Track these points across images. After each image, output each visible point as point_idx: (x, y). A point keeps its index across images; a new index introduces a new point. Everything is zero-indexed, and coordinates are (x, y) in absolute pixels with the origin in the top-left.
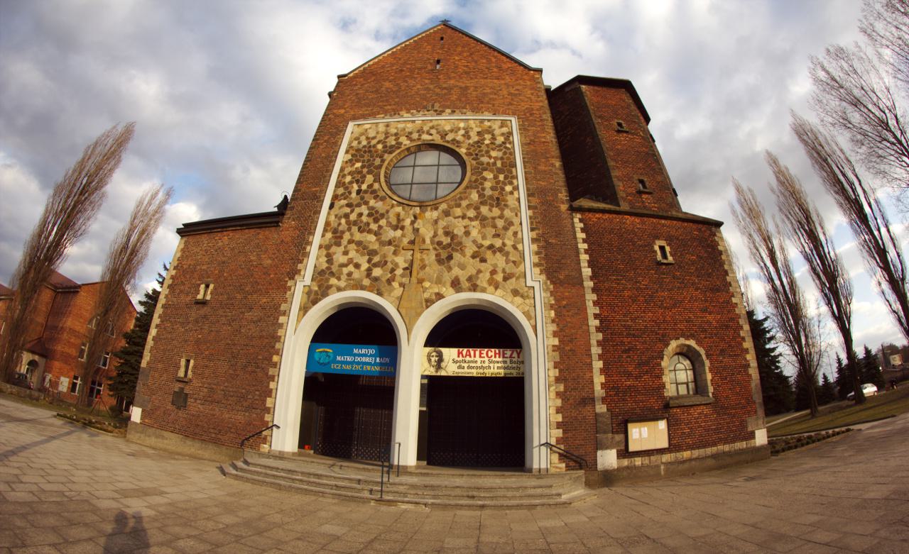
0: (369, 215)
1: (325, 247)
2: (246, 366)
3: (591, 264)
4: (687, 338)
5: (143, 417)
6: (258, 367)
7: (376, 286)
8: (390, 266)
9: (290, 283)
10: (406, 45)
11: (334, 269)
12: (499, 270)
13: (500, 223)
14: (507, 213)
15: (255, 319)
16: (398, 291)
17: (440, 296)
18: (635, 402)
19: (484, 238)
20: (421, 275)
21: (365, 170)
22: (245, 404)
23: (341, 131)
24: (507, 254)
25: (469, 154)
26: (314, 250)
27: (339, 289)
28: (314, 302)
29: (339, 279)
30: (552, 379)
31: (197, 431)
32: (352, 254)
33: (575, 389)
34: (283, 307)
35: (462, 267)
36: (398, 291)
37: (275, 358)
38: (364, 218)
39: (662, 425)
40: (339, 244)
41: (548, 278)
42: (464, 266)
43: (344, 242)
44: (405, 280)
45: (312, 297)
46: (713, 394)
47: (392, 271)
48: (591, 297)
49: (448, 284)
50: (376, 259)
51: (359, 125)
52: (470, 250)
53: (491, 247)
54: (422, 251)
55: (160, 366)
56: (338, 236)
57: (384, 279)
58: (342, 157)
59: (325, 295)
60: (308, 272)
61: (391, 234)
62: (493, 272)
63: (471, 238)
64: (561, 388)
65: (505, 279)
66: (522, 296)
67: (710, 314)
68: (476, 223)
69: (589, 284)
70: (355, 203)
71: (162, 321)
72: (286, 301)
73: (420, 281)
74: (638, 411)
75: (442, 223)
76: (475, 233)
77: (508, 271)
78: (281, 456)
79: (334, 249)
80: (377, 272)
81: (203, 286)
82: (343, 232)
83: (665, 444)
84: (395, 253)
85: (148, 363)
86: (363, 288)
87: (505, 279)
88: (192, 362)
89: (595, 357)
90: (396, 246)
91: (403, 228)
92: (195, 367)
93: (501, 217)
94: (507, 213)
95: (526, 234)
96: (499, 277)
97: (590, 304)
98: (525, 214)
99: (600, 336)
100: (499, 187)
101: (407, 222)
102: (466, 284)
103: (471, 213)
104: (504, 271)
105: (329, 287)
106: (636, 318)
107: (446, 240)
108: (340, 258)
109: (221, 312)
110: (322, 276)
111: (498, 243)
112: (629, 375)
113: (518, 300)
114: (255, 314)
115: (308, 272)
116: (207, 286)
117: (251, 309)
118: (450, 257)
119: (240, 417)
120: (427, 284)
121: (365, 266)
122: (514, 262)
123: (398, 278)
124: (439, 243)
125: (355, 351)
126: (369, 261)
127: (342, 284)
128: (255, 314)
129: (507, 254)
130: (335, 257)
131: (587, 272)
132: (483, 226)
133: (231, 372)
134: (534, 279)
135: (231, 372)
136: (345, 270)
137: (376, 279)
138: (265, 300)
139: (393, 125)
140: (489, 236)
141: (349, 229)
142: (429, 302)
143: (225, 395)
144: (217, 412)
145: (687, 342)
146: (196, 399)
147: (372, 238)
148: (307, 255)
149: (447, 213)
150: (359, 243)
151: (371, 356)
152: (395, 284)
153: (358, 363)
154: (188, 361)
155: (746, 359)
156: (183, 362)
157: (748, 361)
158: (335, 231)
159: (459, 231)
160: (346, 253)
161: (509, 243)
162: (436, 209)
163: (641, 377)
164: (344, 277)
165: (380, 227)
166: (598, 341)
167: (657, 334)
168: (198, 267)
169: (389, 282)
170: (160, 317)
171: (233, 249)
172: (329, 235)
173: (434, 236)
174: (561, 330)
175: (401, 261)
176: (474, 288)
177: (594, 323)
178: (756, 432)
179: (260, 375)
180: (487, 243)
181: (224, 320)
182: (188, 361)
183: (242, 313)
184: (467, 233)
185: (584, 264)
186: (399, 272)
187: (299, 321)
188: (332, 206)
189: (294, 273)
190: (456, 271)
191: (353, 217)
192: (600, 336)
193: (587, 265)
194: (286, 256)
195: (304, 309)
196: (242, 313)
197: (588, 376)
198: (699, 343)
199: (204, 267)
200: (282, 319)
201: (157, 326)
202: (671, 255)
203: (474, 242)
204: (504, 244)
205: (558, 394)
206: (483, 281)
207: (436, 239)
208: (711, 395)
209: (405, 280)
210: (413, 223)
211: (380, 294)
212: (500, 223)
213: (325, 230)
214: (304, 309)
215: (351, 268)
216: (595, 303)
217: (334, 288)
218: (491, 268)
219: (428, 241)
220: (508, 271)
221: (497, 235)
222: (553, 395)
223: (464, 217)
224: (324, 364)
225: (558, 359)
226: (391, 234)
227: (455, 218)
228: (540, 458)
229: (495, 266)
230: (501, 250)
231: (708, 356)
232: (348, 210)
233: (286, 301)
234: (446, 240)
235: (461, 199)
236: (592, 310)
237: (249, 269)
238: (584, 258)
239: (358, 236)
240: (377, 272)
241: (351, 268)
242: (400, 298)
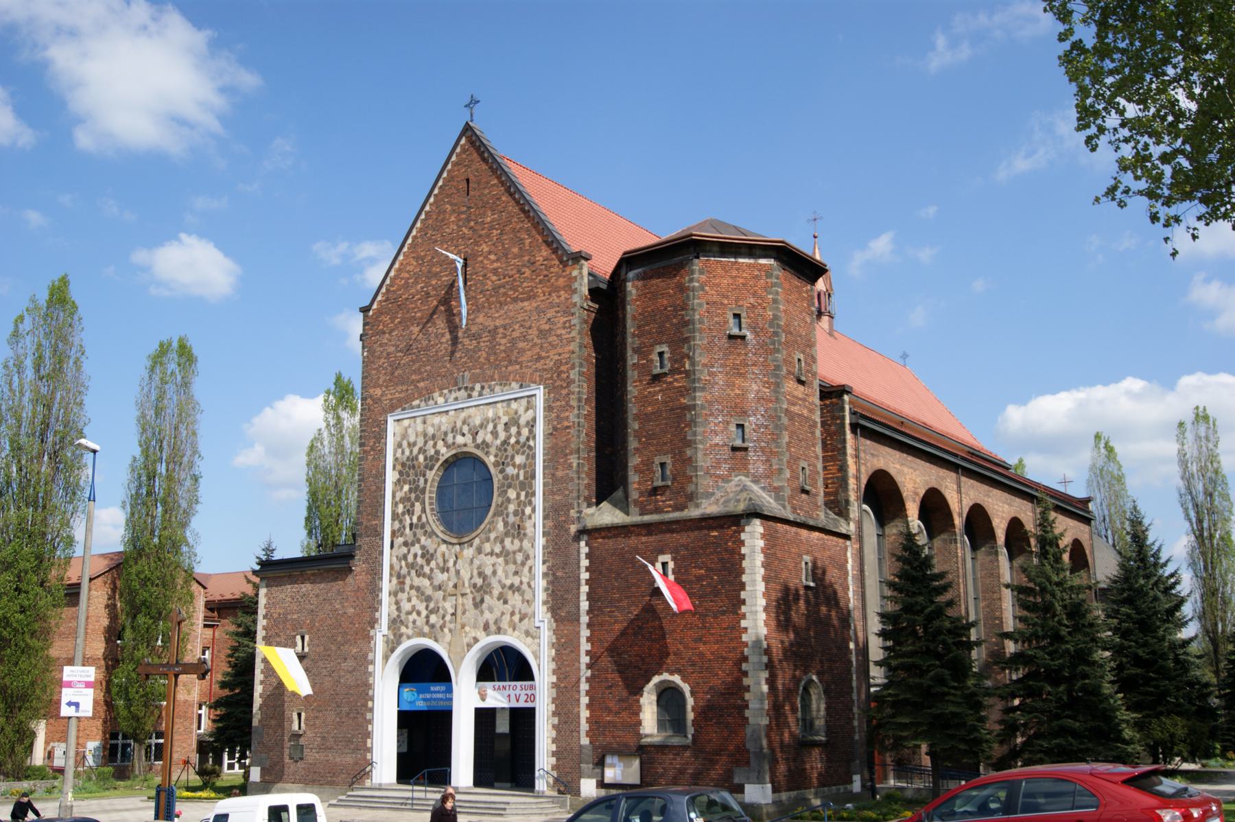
0: (423, 556)
1: (393, 594)
2: (348, 714)
3: (590, 597)
4: (672, 673)
5: (262, 775)
6: (358, 713)
7: (434, 634)
8: (441, 611)
9: (372, 633)
10: (427, 213)
11: (403, 617)
12: (517, 611)
13: (519, 557)
14: (526, 544)
15: (350, 669)
16: (448, 637)
17: (476, 640)
18: (614, 737)
19: (507, 577)
20: (464, 620)
21: (413, 496)
22: (352, 747)
23: (381, 436)
24: (522, 594)
25: (496, 464)
26: (385, 597)
27: (409, 638)
28: (392, 651)
29: (407, 627)
30: (550, 713)
31: (315, 778)
32: (415, 601)
33: (566, 722)
34: (370, 656)
35: (491, 610)
36: (448, 637)
37: (370, 704)
38: (419, 560)
39: (636, 763)
40: (403, 590)
41: (553, 617)
42: (493, 608)
43: (407, 588)
44: (452, 626)
45: (390, 645)
46: (693, 735)
47: (444, 617)
48: (585, 633)
49: (481, 629)
50: (432, 605)
51: (398, 420)
52: (496, 592)
53: (512, 586)
54: (463, 595)
55: (273, 722)
56: (401, 579)
57: (438, 626)
58: (391, 476)
59: (399, 643)
60: (384, 622)
61: (440, 577)
62: (513, 614)
63: (497, 578)
64: (556, 720)
65: (521, 620)
66: (532, 637)
67: (705, 643)
68: (501, 560)
69: (585, 619)
70: (410, 541)
71: (266, 677)
72: (371, 651)
73: (463, 627)
74: (615, 746)
75: (477, 562)
76: (500, 572)
77: (523, 612)
78: (380, 788)
79: (400, 595)
80: (433, 619)
81: (298, 638)
82: (404, 577)
83: (637, 781)
84: (444, 599)
85: (260, 721)
86: (424, 635)
87: (521, 620)
88: (303, 715)
89: (583, 693)
90: (444, 591)
91: (448, 570)
92: (306, 719)
93: (520, 550)
94: (526, 544)
95: (540, 569)
96: (516, 618)
97: (583, 640)
98: (540, 541)
99: (589, 673)
100: (519, 513)
101: (451, 564)
102: (493, 628)
103: (498, 549)
104: (520, 613)
105: (401, 635)
106: (621, 654)
107: (479, 582)
108: (406, 606)
109: (320, 663)
110: (395, 623)
111: (516, 581)
112: (610, 711)
113: (529, 640)
114: (350, 664)
115: (384, 622)
116: (303, 638)
117: (345, 659)
118: (482, 601)
119: (349, 759)
120: (467, 629)
121: (424, 613)
122: (528, 601)
123: (448, 625)
124: (475, 586)
125: (432, 689)
126: (427, 608)
127: (410, 632)
128: (350, 664)
129: (522, 594)
130: (402, 604)
131: (584, 605)
132: (507, 562)
133: (338, 719)
134: (542, 616)
135: (338, 719)
136: (411, 618)
137: (433, 626)
138: (355, 650)
139: (430, 420)
140: (511, 574)
141: (409, 573)
142: (469, 646)
143: (335, 742)
144: (331, 758)
145: (671, 678)
146: (311, 749)
147: (426, 582)
148: (380, 602)
149: (479, 550)
150: (418, 589)
151: (443, 692)
152: (446, 630)
153: (435, 699)
154: (299, 715)
155: (743, 699)
156: (295, 716)
157: (747, 701)
158: (399, 576)
159: (488, 571)
160: (409, 600)
161: (525, 580)
162: (471, 546)
163: (620, 713)
164: (411, 625)
165: (432, 570)
166: (587, 678)
167: (640, 669)
168: (289, 617)
169: (442, 628)
170: (262, 672)
171: (317, 596)
172: (395, 580)
173: (471, 578)
174: (559, 668)
175: (448, 606)
176: (499, 631)
177: (585, 659)
178: (746, 786)
179: (360, 720)
180: (508, 582)
181: (325, 672)
182: (299, 715)
183: (339, 663)
184: (494, 573)
185: (583, 597)
186: (448, 618)
187: (383, 669)
188: (392, 546)
189: (373, 622)
190: (487, 615)
191: (410, 558)
192: (589, 673)
193: (585, 598)
194: (365, 603)
195: (386, 658)
196: (339, 663)
197: (576, 710)
198: (684, 679)
199: (295, 616)
200: (371, 668)
201: (262, 682)
202: (674, 573)
203: (500, 582)
204: (521, 583)
205: (554, 726)
206: (504, 624)
207: (473, 581)
208: (690, 736)
209: (452, 626)
210: (455, 563)
211: (436, 640)
212: (519, 557)
213: (391, 575)
214: (386, 658)
215: (414, 615)
216: (589, 640)
217: (405, 637)
218: (511, 610)
219: (467, 585)
220: (523, 612)
221: (516, 573)
222: (550, 726)
223: (492, 554)
224: (410, 702)
225: (555, 696)
226: (440, 577)
227: (486, 555)
228: (541, 785)
229: (514, 606)
230: (518, 589)
231: (692, 693)
232: (405, 550)
233: (371, 651)
234: (479, 582)
235: (490, 531)
236: (585, 646)
237: (336, 618)
238: (585, 589)
239: (418, 581)
240: (433, 619)
241: (414, 615)
242: (450, 644)
